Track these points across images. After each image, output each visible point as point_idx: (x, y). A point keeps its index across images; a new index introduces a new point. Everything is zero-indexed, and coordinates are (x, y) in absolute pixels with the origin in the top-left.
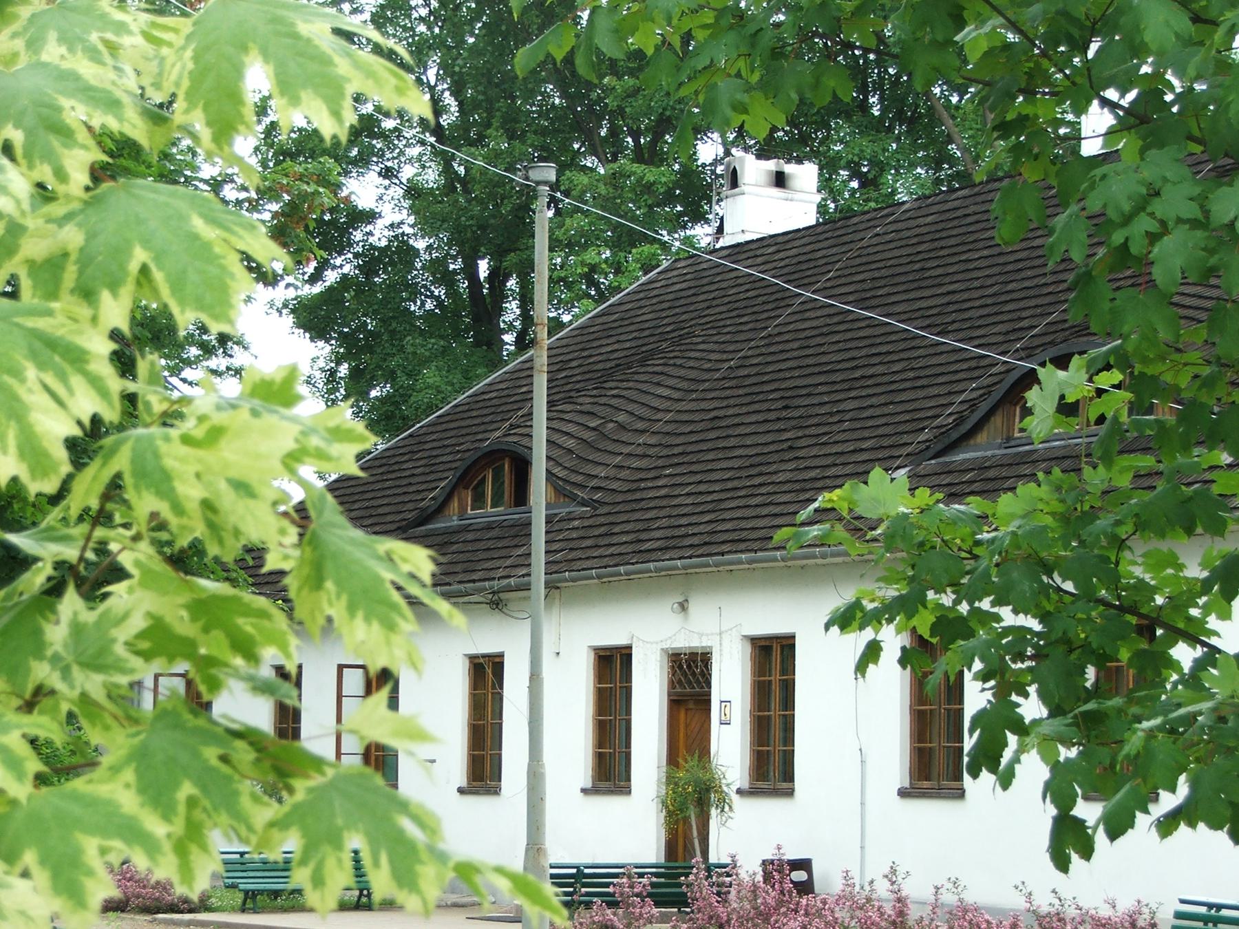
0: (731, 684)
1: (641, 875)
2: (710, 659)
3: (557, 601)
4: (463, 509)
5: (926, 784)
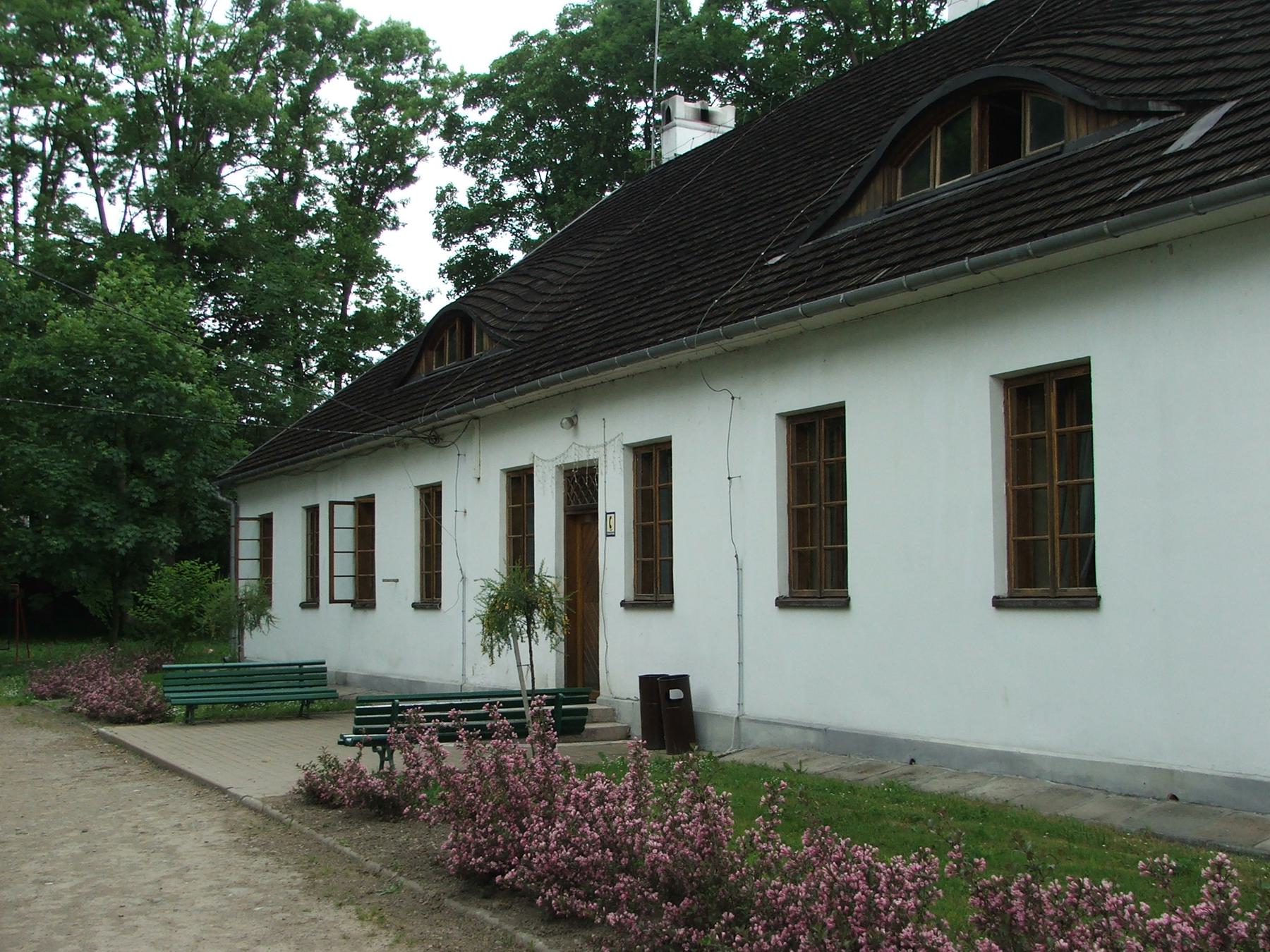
0: (615, 495)
1: (429, 719)
2: (596, 470)
3: (477, 431)
4: (429, 366)
5: (806, 592)
